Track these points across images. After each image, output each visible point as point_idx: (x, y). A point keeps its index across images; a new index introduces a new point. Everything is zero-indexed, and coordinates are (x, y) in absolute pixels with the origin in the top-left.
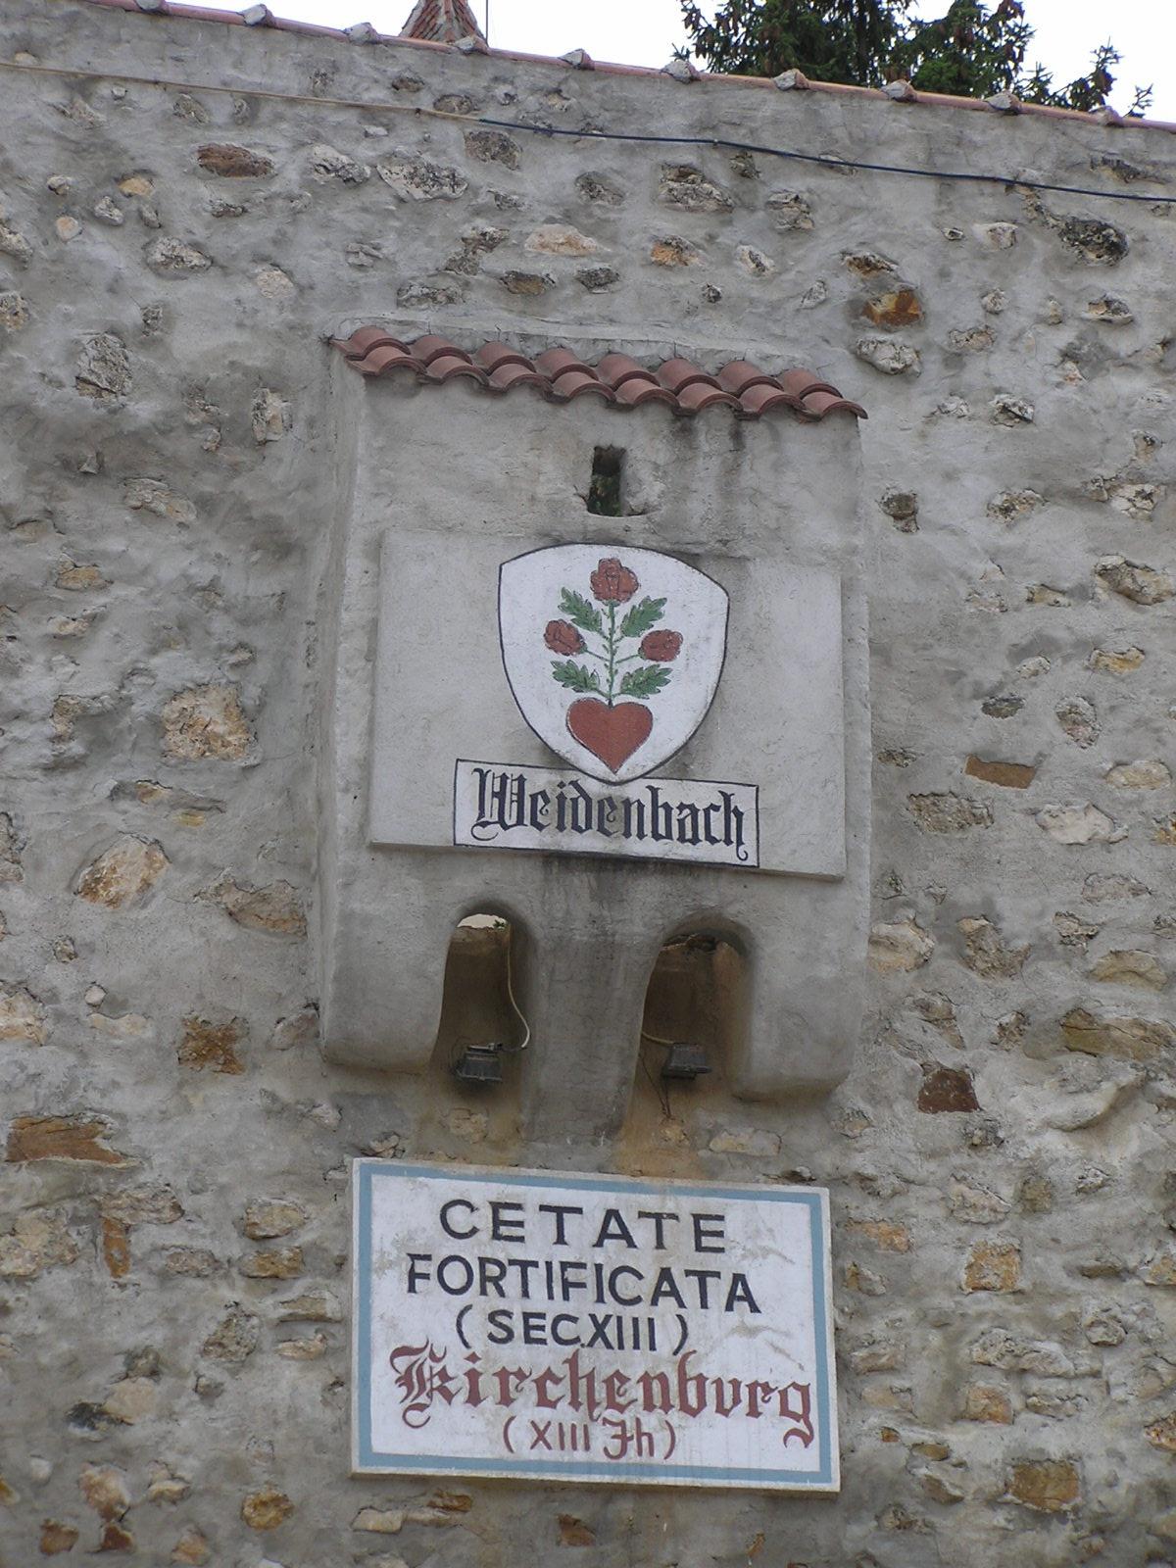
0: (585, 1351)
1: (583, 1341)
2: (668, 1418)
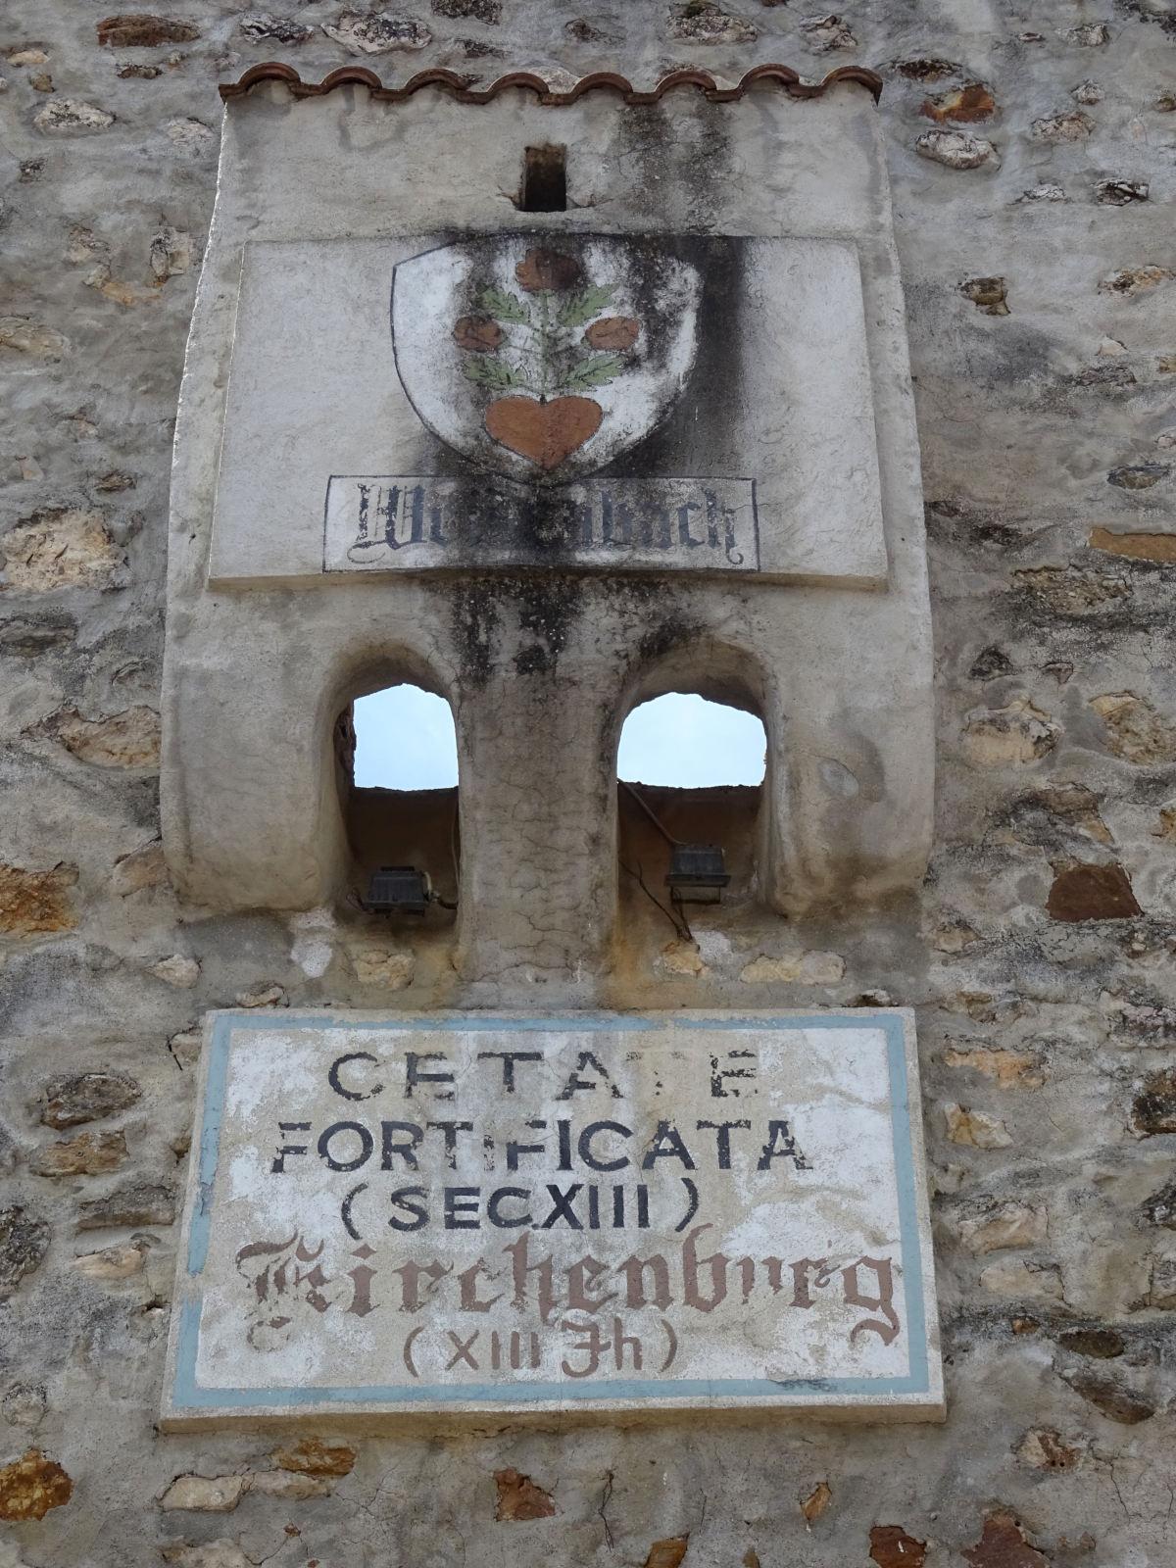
0: (540, 1233)
1: (535, 1222)
2: (665, 1316)
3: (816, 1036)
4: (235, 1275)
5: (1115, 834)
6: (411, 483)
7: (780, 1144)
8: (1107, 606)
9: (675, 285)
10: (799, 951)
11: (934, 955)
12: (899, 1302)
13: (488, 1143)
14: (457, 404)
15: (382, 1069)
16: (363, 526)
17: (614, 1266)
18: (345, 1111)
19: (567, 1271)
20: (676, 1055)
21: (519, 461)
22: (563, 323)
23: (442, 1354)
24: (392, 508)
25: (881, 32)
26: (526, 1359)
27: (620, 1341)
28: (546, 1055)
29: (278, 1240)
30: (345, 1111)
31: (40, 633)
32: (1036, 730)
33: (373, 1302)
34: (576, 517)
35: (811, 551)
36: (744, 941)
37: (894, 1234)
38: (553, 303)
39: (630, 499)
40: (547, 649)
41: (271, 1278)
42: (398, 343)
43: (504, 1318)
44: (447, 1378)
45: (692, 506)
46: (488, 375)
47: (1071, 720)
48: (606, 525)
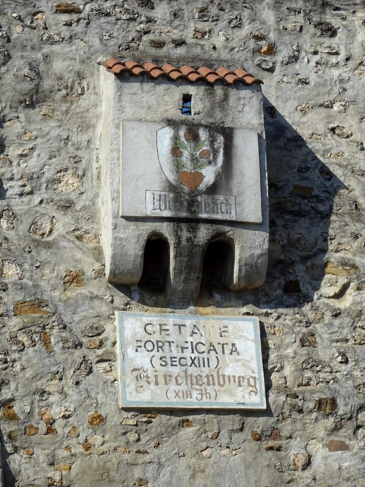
0: (189, 368)
2: (214, 388)
3: (240, 323)
4: (131, 375)
5: (297, 271)
6: (163, 193)
7: (234, 349)
8: (296, 208)
9: (218, 141)
10: (234, 300)
11: (261, 302)
12: (258, 386)
13: (177, 346)
14: (172, 172)
15: (155, 327)
16: (154, 204)
17: (204, 376)
18: (148, 337)
19: (195, 377)
20: (213, 326)
21: (186, 189)
22: (194, 150)
23: (174, 395)
24: (160, 200)
25: (248, 22)
26: (189, 397)
27: (206, 393)
28: (187, 325)
29: (139, 368)
30: (148, 337)
31: (66, 205)
32: (281, 243)
33: (159, 383)
34: (199, 205)
35: (246, 216)
36: (223, 296)
37: (256, 371)
38: (192, 144)
39: (210, 201)
40: (193, 238)
41: (139, 377)
42: (159, 153)
43: (184, 387)
44: (175, 400)
45: (223, 203)
46: (179, 164)
47: (288, 240)
48: (205, 207)
